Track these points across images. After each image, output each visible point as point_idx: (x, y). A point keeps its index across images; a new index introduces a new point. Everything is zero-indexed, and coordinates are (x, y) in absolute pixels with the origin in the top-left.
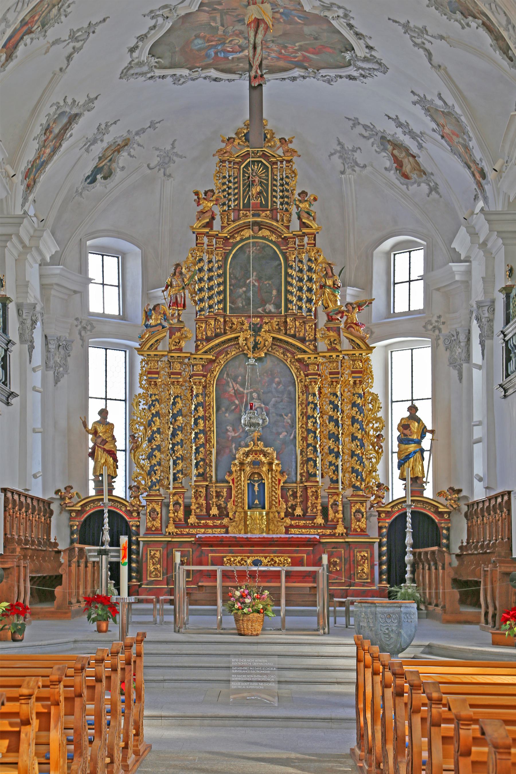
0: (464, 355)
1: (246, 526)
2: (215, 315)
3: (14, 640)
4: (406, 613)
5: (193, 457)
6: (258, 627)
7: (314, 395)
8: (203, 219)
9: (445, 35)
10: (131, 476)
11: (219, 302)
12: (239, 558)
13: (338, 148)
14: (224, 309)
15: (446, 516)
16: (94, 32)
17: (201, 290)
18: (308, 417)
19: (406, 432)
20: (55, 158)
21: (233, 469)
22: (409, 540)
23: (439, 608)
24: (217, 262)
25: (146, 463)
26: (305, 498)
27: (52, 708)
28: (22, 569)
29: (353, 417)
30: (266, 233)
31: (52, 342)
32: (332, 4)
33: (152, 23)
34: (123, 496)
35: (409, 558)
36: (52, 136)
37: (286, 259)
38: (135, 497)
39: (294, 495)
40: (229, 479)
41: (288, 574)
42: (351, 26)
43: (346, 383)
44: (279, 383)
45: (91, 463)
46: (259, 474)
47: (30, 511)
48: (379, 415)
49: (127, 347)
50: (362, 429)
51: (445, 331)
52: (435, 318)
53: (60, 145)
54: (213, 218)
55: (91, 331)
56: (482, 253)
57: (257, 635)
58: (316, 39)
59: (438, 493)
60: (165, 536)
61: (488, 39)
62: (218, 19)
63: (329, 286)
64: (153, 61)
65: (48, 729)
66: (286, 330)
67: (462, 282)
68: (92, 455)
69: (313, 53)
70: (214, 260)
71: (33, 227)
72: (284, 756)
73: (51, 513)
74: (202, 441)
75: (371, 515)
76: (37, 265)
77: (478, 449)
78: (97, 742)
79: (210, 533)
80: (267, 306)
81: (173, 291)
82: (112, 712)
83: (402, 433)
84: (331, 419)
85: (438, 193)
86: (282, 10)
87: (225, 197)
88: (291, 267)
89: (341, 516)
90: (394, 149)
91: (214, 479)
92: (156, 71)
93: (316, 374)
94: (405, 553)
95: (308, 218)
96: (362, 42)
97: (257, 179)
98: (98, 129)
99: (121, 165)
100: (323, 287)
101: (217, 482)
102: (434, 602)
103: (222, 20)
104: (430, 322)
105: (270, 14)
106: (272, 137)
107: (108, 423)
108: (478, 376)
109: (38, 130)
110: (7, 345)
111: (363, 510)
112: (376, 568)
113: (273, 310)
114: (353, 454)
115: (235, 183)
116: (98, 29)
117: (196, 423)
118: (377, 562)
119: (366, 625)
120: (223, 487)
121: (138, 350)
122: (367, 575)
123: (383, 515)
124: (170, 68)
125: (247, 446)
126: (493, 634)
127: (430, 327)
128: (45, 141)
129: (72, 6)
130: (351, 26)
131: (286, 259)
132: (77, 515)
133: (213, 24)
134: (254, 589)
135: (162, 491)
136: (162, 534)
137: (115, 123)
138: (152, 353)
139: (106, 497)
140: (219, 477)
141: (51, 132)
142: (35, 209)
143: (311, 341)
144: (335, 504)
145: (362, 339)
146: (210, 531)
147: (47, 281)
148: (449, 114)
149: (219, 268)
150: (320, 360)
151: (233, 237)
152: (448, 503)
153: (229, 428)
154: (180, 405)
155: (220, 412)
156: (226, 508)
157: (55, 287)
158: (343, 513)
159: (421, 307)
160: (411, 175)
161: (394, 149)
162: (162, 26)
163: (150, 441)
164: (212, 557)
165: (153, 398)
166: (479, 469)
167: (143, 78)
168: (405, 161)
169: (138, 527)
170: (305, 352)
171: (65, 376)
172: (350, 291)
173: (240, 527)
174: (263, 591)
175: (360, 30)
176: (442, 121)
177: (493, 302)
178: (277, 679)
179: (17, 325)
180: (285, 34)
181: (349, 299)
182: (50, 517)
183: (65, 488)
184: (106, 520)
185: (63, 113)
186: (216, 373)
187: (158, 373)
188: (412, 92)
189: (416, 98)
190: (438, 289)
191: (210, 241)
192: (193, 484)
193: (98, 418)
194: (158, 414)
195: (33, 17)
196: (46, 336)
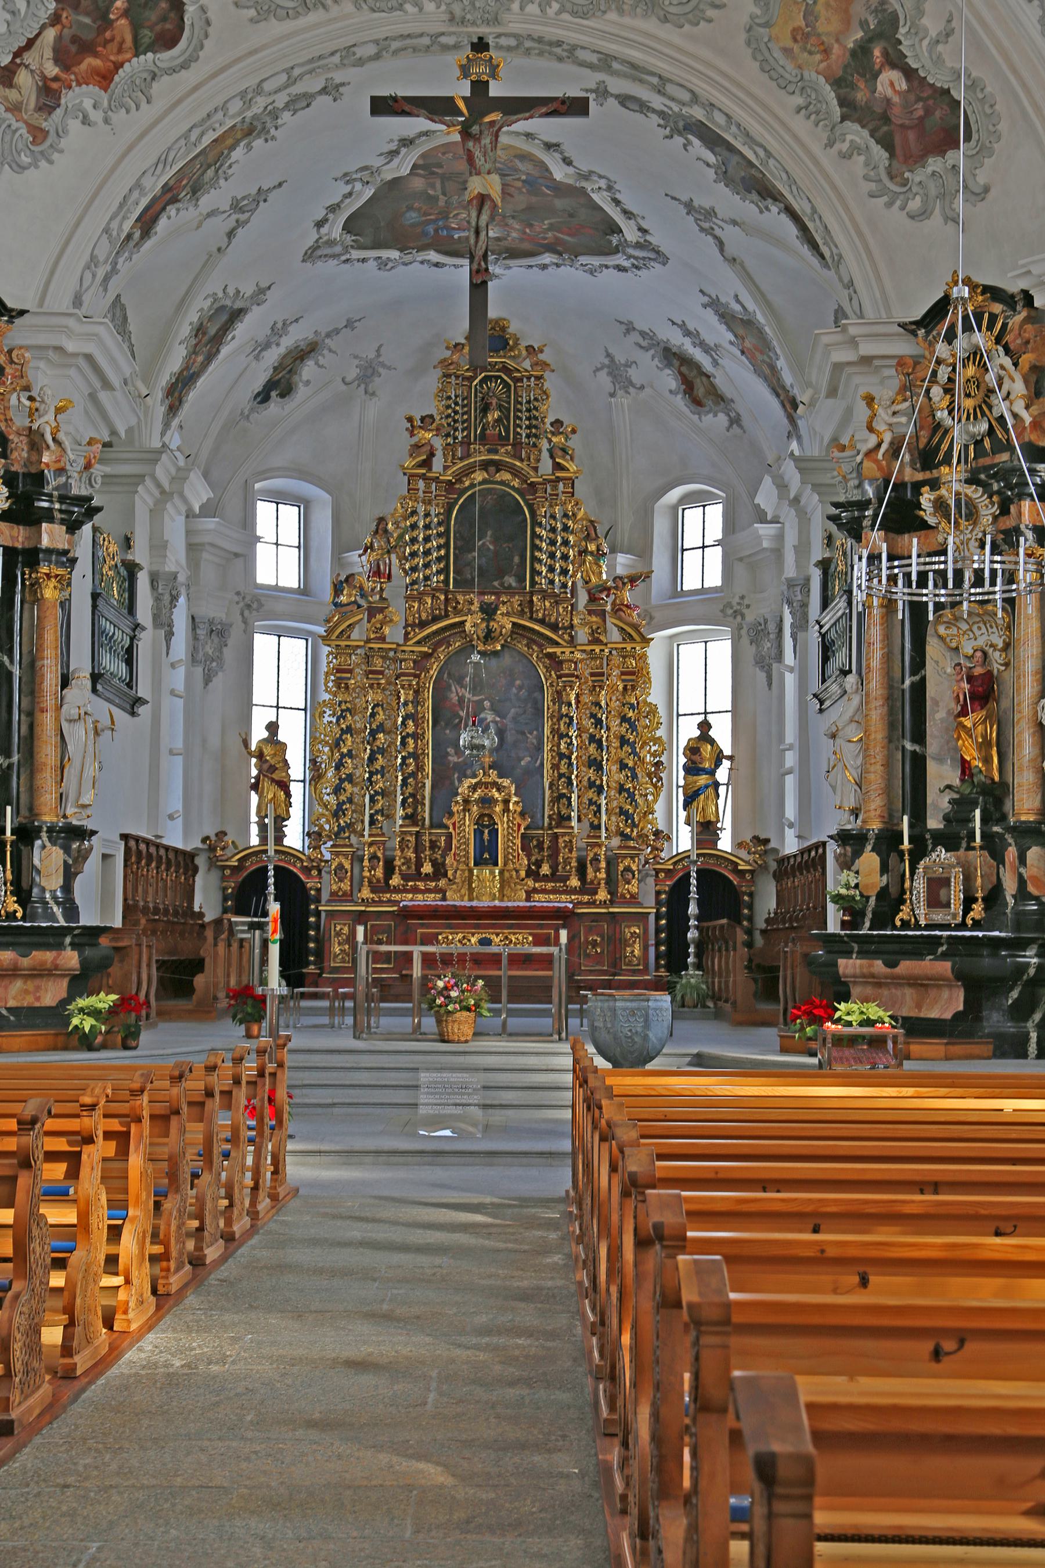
0: (774, 652)
1: (471, 890)
2: (433, 589)
3: (126, 1047)
4: (655, 1009)
5: (399, 792)
6: (468, 1031)
7: (570, 704)
8: (418, 455)
10: (311, 818)
11: (439, 572)
12: (460, 936)
13: (606, 361)
14: (446, 582)
15: (748, 877)
16: (265, 201)
17: (414, 554)
18: (561, 736)
19: (694, 758)
20: (211, 368)
21: (455, 809)
22: (693, 909)
23: (728, 1005)
24: (437, 515)
25: (332, 800)
26: (555, 851)
27: (133, 1125)
28: (144, 949)
29: (622, 737)
30: (506, 476)
31: (201, 626)
32: (591, 172)
33: (347, 189)
34: (298, 846)
35: (692, 934)
36: (206, 338)
37: (533, 513)
38: (315, 848)
39: (540, 846)
40: (449, 823)
42: (617, 202)
43: (613, 688)
44: (520, 688)
45: (254, 798)
47: (163, 867)
48: (659, 733)
49: (310, 633)
50: (634, 753)
51: (750, 617)
52: (737, 599)
53: (218, 351)
54: (432, 454)
55: (257, 610)
56: (793, 512)
57: (466, 1041)
58: (571, 216)
59: (739, 845)
60: (357, 904)
61: (792, 230)
62: (438, 185)
63: (592, 553)
64: (349, 239)
65: (127, 1153)
66: (531, 612)
67: (772, 550)
68: (255, 787)
69: (569, 235)
70: (433, 513)
71: (175, 465)
72: (476, 1201)
73: (196, 869)
75: (647, 875)
76: (183, 518)
77: (790, 782)
78: (206, 1178)
79: (422, 900)
80: (506, 578)
82: (234, 1139)
83: (689, 759)
85: (740, 426)
86: (524, 177)
87: (449, 425)
88: (540, 525)
89: (604, 876)
90: (681, 365)
91: (427, 822)
92: (353, 252)
93: (572, 675)
94: (688, 928)
95: (563, 458)
96: (632, 222)
97: (494, 401)
98: (272, 329)
99: (305, 378)
100: (583, 552)
101: (432, 826)
102: (724, 995)
103: (443, 187)
104: (729, 605)
105: (498, 188)
106: (516, 344)
107: (279, 743)
108: (790, 681)
109: (186, 330)
110: (134, 630)
111: (634, 868)
112: (652, 951)
113: (514, 584)
114: (621, 789)
115: (463, 406)
116: (271, 197)
117: (404, 743)
118: (652, 942)
120: (440, 835)
121: (324, 638)
122: (638, 959)
123: (662, 875)
124: (373, 248)
125: (474, 776)
126: (781, 1037)
127: (730, 612)
128: (196, 345)
129: (234, 166)
130: (617, 202)
131: (533, 513)
132: (232, 874)
133: (431, 192)
134: (464, 979)
135: (354, 839)
136: (352, 901)
137: (297, 321)
138: (343, 643)
139: (271, 848)
140: (435, 820)
141: (204, 334)
142: (182, 438)
143: (565, 628)
144: (596, 859)
145: (636, 627)
146: (420, 896)
147: (197, 540)
148: (749, 323)
149: (439, 524)
150: (578, 655)
151: (459, 481)
152: (751, 858)
154: (381, 717)
155: (438, 728)
156: (443, 864)
157: (207, 547)
158: (608, 872)
159: (719, 583)
160: (705, 401)
161: (681, 365)
162: (360, 194)
164: (422, 934)
165: (344, 707)
166: (790, 812)
167: (335, 262)
169: (319, 890)
170: (557, 644)
171: (220, 674)
172: (622, 559)
173: (463, 891)
174: (476, 980)
175: (629, 207)
176: (741, 331)
177: (808, 580)
178: (482, 1102)
179: (150, 602)
180: (529, 208)
181: (620, 571)
182: (194, 876)
183: (217, 835)
184: (271, 881)
185: (223, 308)
186: (434, 672)
187: (350, 671)
188: (701, 291)
189: (706, 299)
190: (741, 559)
191: (428, 486)
192: (397, 829)
193: (265, 734)
194: (349, 730)
195: (180, 181)
196: (193, 618)
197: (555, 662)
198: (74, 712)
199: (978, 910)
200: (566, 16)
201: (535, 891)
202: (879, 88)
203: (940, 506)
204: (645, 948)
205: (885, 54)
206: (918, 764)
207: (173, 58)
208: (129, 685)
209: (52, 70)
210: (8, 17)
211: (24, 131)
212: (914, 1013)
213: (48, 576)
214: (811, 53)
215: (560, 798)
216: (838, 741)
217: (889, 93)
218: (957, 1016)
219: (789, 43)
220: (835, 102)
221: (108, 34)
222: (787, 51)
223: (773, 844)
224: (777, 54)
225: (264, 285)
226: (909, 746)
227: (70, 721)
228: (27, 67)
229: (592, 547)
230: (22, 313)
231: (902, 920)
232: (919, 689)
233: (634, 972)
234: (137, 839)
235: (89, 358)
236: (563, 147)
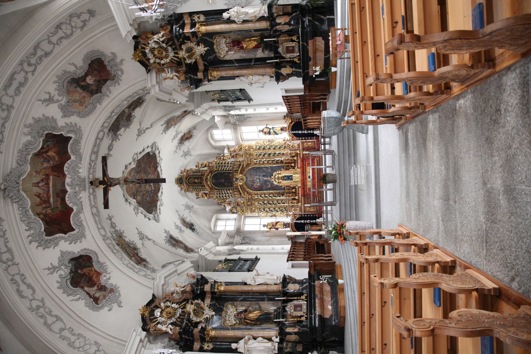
14: (231, 189)
18: (264, 163)
22: (300, 132)
25: (279, 212)
30: (209, 177)
35: (305, 132)
36: (176, 244)
37: (216, 171)
41: (313, 165)
42: (140, 153)
44: (254, 172)
46: (282, 177)
50: (267, 146)
58: (146, 163)
62: (139, 193)
64: (153, 213)
68: (277, 229)
74: (272, 195)
81: (226, 205)
84: (264, 156)
117: (267, 197)
153: (268, 187)
154: (261, 202)
163: (272, 211)
168: (187, 137)
169: (299, 214)
176: (170, 125)
177: (224, 106)
182: (297, 242)
186: (251, 191)
193: (266, 227)
197: (248, 165)
198: (253, 281)
199: (294, 38)
200: (82, 162)
201: (298, 167)
202: (91, 83)
203: (190, 57)
204: (309, 142)
205: (82, 81)
207: (94, 257)
208: (252, 260)
209: (95, 288)
210: (81, 299)
211: (110, 295)
212: (323, 53)
213: (218, 289)
214: (85, 101)
215: (277, 163)
216: (253, 82)
217: (92, 80)
218: (323, 39)
219: (83, 107)
220: (97, 95)
221: (87, 274)
222: (86, 107)
223: (285, 115)
224: (87, 110)
225: (164, 231)
226: (253, 63)
227: (255, 282)
228: (94, 294)
229: (222, 158)
230: (153, 295)
232: (237, 61)
233: (315, 144)
234: (288, 257)
235: (165, 278)
236: (126, 164)
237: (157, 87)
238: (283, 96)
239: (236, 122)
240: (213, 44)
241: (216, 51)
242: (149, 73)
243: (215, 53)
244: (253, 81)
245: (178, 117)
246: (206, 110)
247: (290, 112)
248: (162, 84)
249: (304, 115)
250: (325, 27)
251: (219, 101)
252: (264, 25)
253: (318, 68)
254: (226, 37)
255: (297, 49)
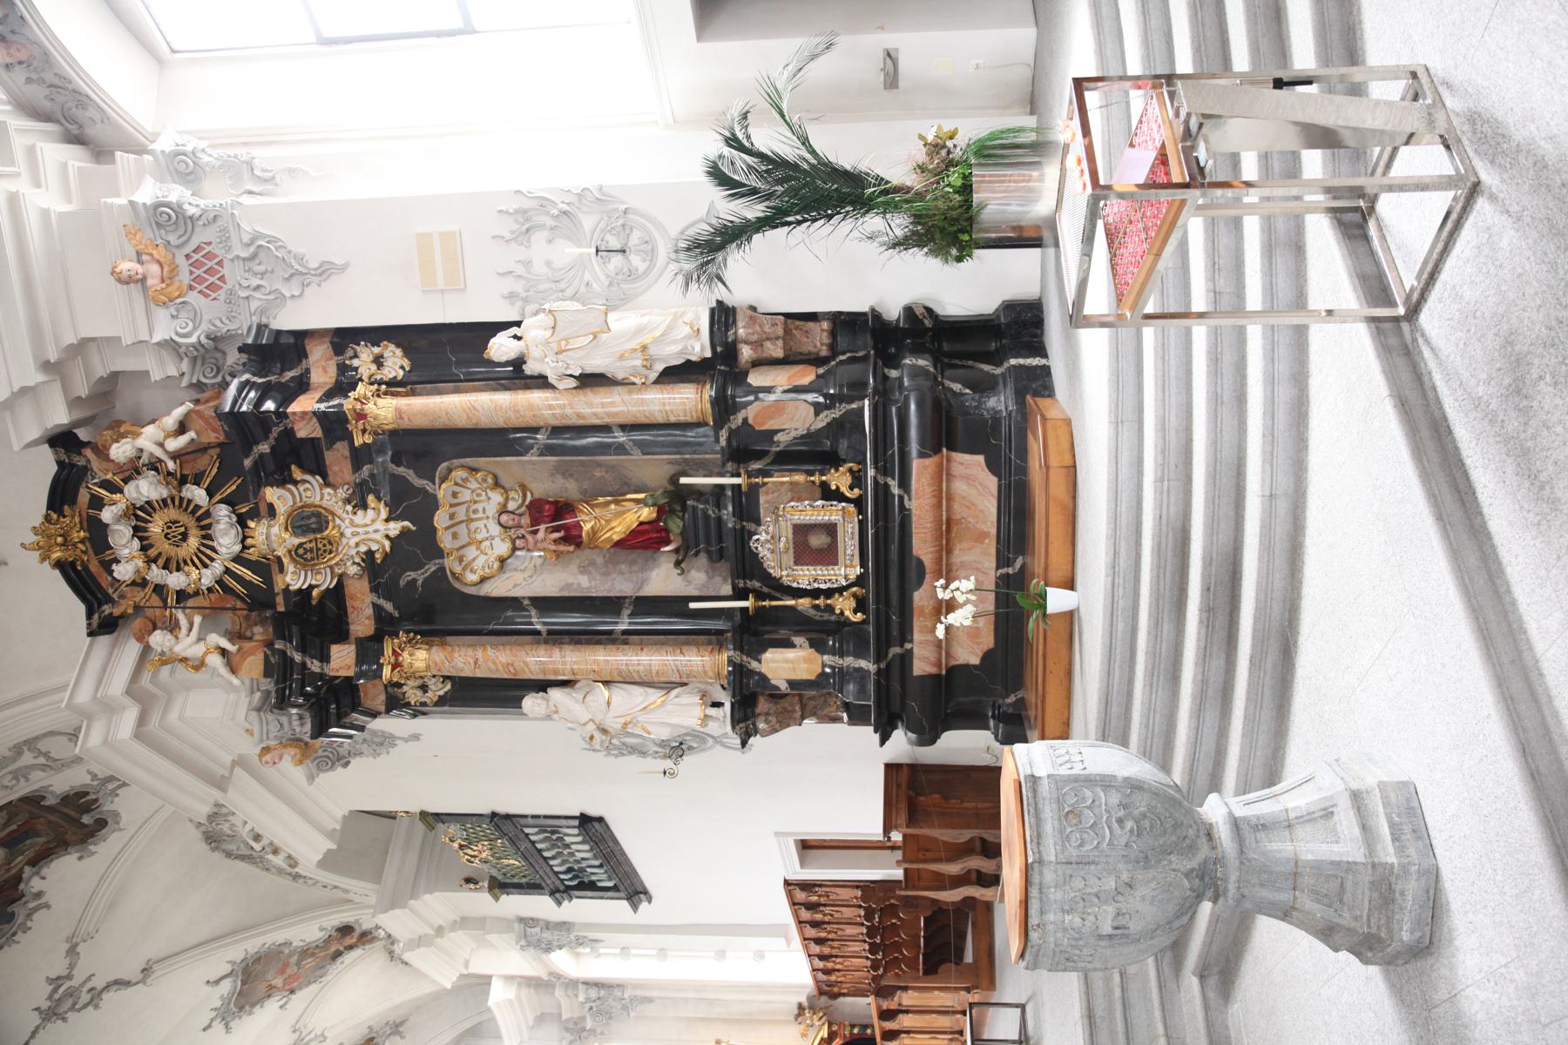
9: (67, 946)
15: (835, 1028)
119: (1110, 909)
176: (261, 988)
188: (204, 1030)
199: (839, 479)
206: (646, 605)
218: (993, 467)
231: (851, 488)
237: (131, 715)
238: (787, 883)
239: (583, 1018)
240: (432, 504)
241: (445, 541)
242: (104, 641)
243: (440, 553)
244: (613, 712)
245: (306, 952)
246: (440, 931)
247: (827, 990)
248: (165, 711)
249: (884, 983)
250: (1000, 403)
251: (500, 886)
252: (688, 400)
253: (963, 586)
254: (506, 480)
255: (848, 543)
